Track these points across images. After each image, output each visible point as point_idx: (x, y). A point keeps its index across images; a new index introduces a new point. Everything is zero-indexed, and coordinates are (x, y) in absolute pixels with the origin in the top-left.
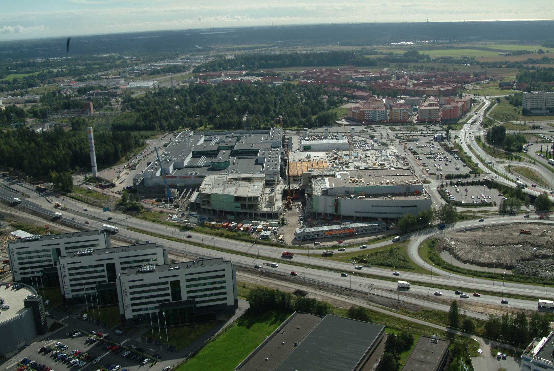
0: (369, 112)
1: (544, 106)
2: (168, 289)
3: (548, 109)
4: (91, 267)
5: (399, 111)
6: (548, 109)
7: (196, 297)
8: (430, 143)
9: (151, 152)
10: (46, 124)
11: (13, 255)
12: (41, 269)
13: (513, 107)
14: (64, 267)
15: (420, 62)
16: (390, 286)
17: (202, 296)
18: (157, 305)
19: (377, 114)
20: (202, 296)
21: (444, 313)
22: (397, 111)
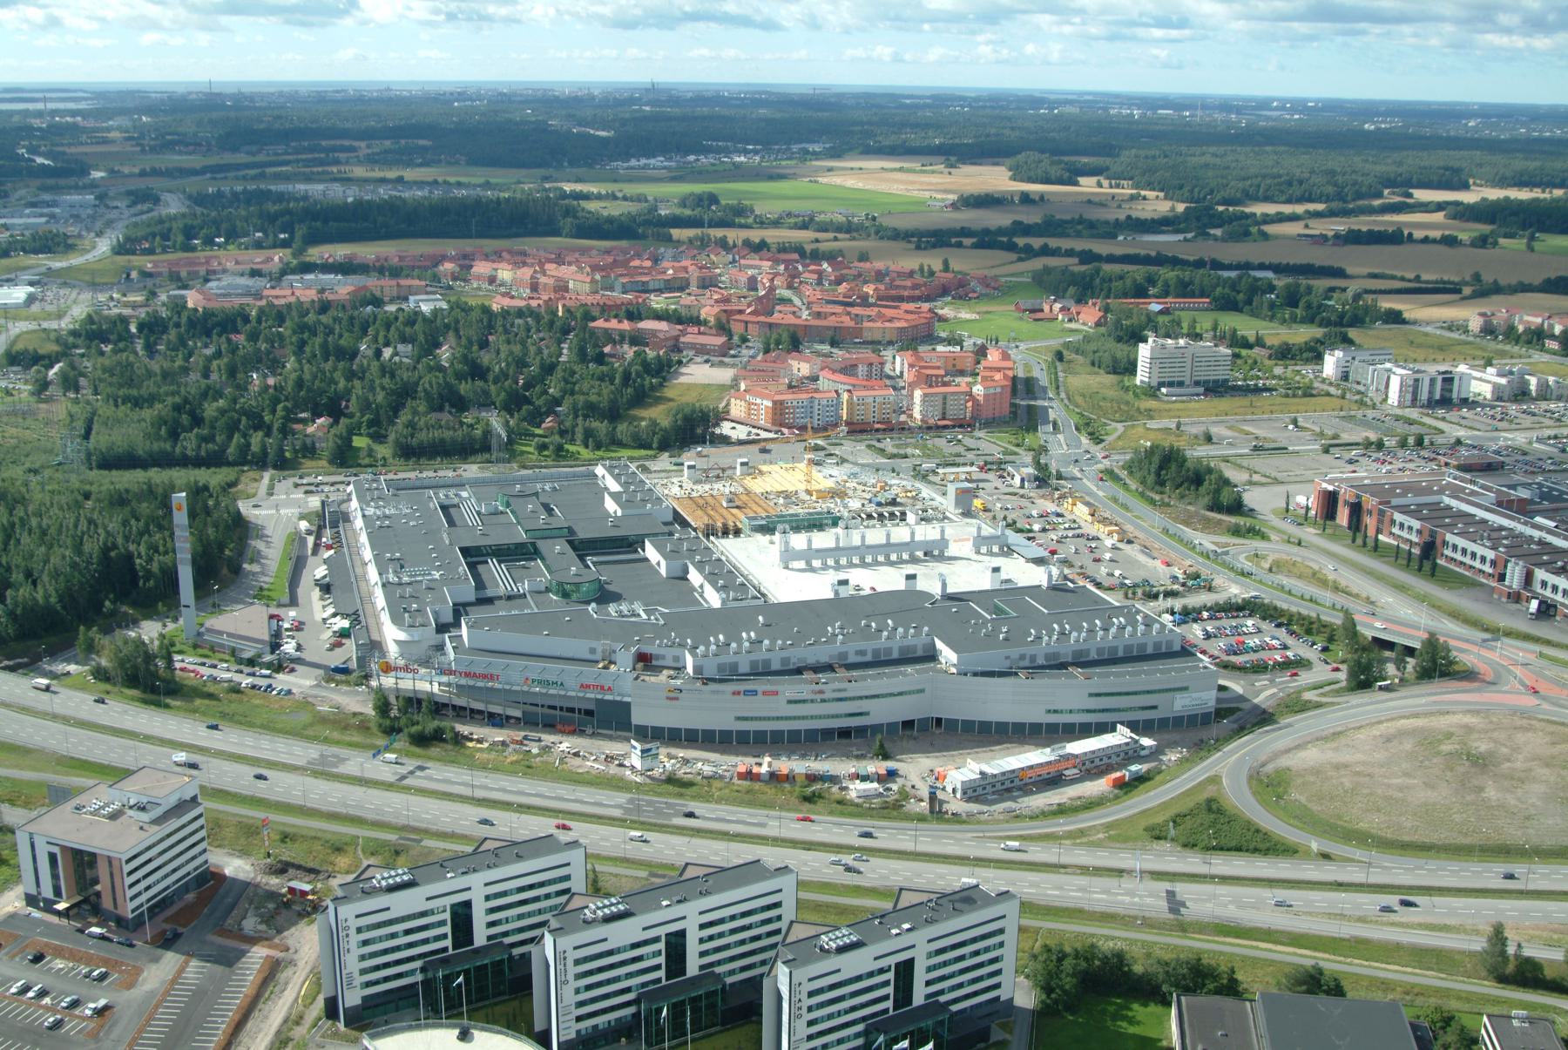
0: (795, 403)
1: (1188, 374)
2: (445, 936)
3: (1197, 383)
4: (871, 974)
5: (871, 400)
6: (1197, 383)
7: (941, 992)
8: (1434, 459)
9: (725, 527)
10: (1120, 169)
11: (347, 936)
12: (418, 964)
13: (1112, 378)
14: (565, 959)
15: (741, 226)
16: (1148, 899)
17: (953, 988)
18: (860, 1027)
19: (817, 407)
20: (953, 988)
21: (1472, 954)
22: (866, 400)
